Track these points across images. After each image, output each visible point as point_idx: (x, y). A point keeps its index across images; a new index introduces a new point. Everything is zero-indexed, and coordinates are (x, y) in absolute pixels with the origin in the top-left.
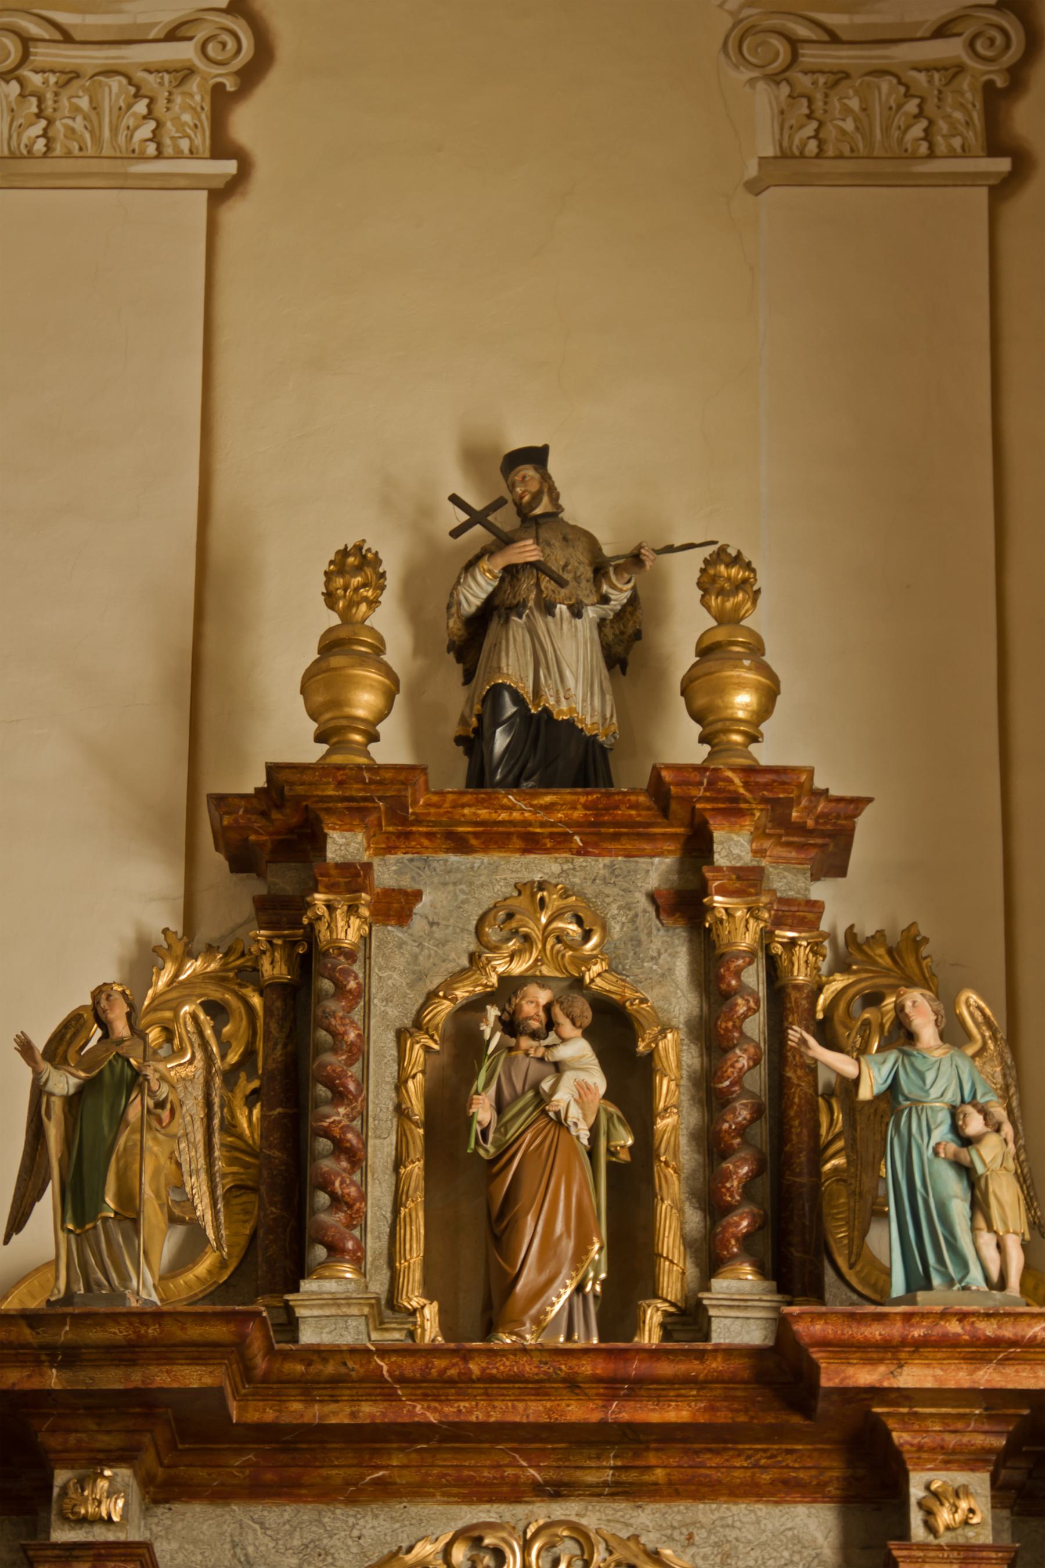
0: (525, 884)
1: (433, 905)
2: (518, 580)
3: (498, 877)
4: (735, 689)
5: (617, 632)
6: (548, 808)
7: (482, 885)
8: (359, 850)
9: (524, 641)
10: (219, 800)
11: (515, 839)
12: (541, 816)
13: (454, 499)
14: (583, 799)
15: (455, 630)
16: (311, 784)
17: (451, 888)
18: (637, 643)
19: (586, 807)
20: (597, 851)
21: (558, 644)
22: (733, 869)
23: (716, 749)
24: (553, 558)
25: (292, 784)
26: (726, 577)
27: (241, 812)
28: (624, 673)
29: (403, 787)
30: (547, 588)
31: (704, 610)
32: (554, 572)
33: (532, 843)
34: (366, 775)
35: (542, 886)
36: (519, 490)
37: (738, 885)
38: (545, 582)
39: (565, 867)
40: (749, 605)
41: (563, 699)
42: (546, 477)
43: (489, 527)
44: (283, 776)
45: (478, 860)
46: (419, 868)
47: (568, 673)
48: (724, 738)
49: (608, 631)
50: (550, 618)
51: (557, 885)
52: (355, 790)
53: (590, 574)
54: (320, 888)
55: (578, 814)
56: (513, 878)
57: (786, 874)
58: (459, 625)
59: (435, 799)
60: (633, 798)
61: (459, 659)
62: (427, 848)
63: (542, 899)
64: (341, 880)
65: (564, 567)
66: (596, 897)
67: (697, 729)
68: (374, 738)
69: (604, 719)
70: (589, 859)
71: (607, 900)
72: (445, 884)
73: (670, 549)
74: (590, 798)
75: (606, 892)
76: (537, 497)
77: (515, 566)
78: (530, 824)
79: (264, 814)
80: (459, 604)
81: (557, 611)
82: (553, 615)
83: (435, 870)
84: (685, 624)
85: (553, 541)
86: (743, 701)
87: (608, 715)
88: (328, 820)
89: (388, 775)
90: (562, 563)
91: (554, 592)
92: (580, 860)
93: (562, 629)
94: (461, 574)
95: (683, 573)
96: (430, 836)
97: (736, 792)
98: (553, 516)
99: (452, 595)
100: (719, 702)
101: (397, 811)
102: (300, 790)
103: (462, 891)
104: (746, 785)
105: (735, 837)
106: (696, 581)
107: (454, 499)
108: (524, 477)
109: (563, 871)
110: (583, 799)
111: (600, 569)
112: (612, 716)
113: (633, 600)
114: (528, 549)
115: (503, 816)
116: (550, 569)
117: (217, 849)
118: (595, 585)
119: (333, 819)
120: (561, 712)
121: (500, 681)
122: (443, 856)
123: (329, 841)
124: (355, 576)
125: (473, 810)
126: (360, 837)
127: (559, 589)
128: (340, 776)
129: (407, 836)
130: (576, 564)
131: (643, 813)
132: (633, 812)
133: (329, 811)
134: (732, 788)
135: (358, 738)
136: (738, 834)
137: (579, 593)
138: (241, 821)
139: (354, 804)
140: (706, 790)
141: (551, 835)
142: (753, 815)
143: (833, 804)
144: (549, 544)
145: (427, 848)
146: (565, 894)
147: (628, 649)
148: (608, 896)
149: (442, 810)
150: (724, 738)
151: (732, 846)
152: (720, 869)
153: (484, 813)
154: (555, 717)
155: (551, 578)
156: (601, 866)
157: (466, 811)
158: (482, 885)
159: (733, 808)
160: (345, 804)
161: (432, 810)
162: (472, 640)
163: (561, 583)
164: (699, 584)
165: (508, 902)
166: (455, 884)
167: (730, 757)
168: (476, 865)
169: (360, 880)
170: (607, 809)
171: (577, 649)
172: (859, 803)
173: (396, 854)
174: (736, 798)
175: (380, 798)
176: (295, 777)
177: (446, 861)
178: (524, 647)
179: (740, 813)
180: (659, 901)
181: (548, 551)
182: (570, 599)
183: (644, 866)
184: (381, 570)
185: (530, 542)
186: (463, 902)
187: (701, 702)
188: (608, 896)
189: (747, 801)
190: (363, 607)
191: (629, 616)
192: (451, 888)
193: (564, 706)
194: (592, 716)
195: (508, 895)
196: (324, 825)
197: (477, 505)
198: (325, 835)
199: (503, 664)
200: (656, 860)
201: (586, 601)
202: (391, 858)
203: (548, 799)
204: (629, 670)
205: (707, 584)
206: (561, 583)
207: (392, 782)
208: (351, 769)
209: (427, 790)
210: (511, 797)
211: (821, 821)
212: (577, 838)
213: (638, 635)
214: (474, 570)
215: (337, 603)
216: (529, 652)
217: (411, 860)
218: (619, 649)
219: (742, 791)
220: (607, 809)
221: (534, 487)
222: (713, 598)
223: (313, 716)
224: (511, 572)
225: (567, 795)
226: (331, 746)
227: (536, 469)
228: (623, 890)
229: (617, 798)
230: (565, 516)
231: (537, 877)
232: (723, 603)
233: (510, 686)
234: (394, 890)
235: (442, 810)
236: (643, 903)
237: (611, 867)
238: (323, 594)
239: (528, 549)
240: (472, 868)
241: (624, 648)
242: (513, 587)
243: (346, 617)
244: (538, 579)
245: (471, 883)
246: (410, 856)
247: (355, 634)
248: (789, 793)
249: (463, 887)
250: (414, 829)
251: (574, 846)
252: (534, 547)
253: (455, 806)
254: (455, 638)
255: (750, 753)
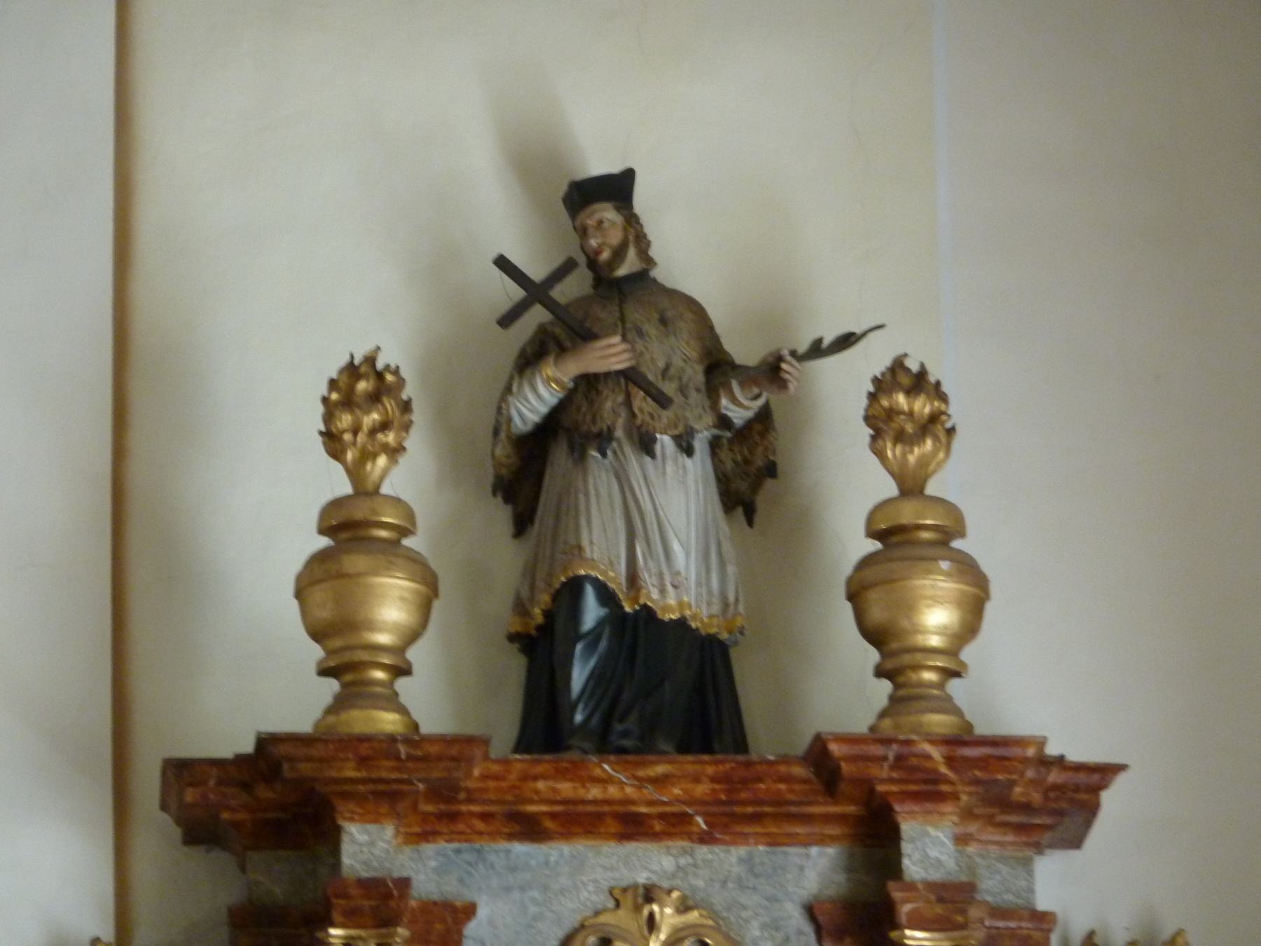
0: (625, 890)
1: (491, 923)
2: (598, 392)
3: (584, 879)
4: (929, 606)
5: (739, 458)
6: (660, 782)
7: (562, 891)
8: (388, 851)
9: (610, 496)
10: (180, 771)
11: (609, 820)
12: (649, 792)
13: (503, 263)
14: (710, 770)
15: (503, 459)
16: (320, 760)
17: (516, 895)
18: (769, 483)
19: (713, 780)
20: (727, 838)
21: (661, 500)
22: (932, 886)
23: (902, 692)
24: (647, 356)
25: (292, 760)
26: (907, 408)
27: (212, 783)
28: (750, 523)
29: (453, 764)
30: (641, 410)
31: (874, 460)
32: (651, 384)
33: (633, 826)
34: (403, 749)
35: (650, 894)
36: (593, 243)
37: (939, 909)
38: (641, 401)
39: (682, 861)
40: (941, 455)
41: (670, 588)
42: (632, 220)
43: (550, 305)
44: (281, 750)
45: (557, 852)
46: (469, 864)
47: (676, 547)
48: (913, 676)
49: (725, 455)
50: (647, 459)
51: (669, 892)
52: (385, 770)
53: (700, 378)
54: (337, 917)
55: (702, 789)
56: (606, 879)
57: (1000, 866)
58: (509, 449)
59: (495, 768)
60: (783, 769)
61: (508, 499)
62: (481, 833)
63: (651, 916)
64: (366, 903)
65: (665, 373)
66: (729, 909)
67: (873, 656)
68: (402, 670)
69: (726, 605)
70: (716, 849)
71: (744, 914)
72: (508, 889)
73: (817, 350)
74: (721, 768)
75: (742, 900)
76: (619, 254)
77: (596, 376)
78: (633, 802)
79: (246, 787)
80: (510, 419)
81: (658, 448)
82: (651, 454)
83: (492, 866)
84: (846, 483)
85: (646, 327)
86: (936, 619)
87: (731, 598)
88: (343, 807)
89: (434, 749)
90: (661, 364)
91: (652, 416)
92: (703, 851)
93: (664, 473)
94: (511, 379)
95: (841, 388)
96: (484, 817)
97: (935, 771)
98: (642, 278)
99: (499, 409)
100: (904, 623)
101: (445, 792)
102: (306, 769)
103: (534, 901)
104: (950, 761)
105: (932, 831)
106: (862, 413)
107: (503, 263)
108: (601, 222)
109: (679, 867)
110: (710, 770)
111: (718, 367)
112: (737, 600)
113: (764, 416)
114: (613, 351)
115: (595, 792)
116: (645, 378)
117: (164, 807)
118: (709, 397)
119: (352, 806)
120: (667, 608)
121: (582, 572)
122: (503, 845)
123: (345, 838)
124: (368, 412)
125: (551, 783)
126: (389, 831)
127: (660, 411)
128: (364, 750)
129: (453, 817)
130: (681, 363)
131: (797, 787)
132: (782, 787)
133: (345, 796)
134: (928, 764)
135: (379, 675)
136: (936, 827)
137: (688, 414)
138: (212, 796)
139: (381, 787)
140: (892, 768)
141: (662, 816)
142: (958, 799)
143: (1070, 774)
144: (640, 333)
145: (481, 833)
146: (684, 907)
147: (756, 486)
148: (745, 908)
149: (504, 784)
150: (913, 676)
151: (930, 847)
152: (911, 887)
153: (566, 788)
154: (660, 615)
155: (648, 393)
156: (734, 860)
157: (541, 785)
158: (562, 891)
159: (929, 792)
160: (371, 787)
161: (491, 784)
162: (527, 475)
163: (662, 401)
164: (869, 419)
165: (603, 919)
166: (522, 889)
167: (923, 711)
168: (552, 859)
169: (393, 904)
170: (744, 781)
171: (687, 503)
172: (1105, 773)
173: (435, 841)
174: (937, 779)
175: (420, 780)
176: (301, 751)
177: (508, 852)
178: (612, 506)
179: (940, 797)
180: (821, 918)
181: (640, 346)
182: (676, 426)
183: (797, 860)
184: (404, 397)
185: (616, 339)
186: (535, 918)
187: (877, 614)
188: (745, 908)
189: (952, 783)
190: (382, 461)
191: (757, 438)
192: (516, 895)
193: (672, 601)
194: (709, 604)
195: (600, 907)
196: (337, 816)
197: (537, 272)
198: (338, 830)
199: (585, 543)
200: (814, 850)
201: (697, 426)
202: (429, 848)
203: (660, 769)
204: (758, 519)
205: (881, 422)
206: (662, 401)
207: (439, 758)
208: (381, 741)
209: (486, 758)
210: (606, 767)
211: (1052, 795)
212: (699, 820)
213: (771, 470)
214: (533, 374)
215: (343, 451)
216: (619, 512)
217: (458, 851)
218: (742, 486)
219: (943, 769)
220: (744, 781)
221: (615, 237)
222: (889, 445)
223: (318, 634)
224: (589, 383)
225: (689, 763)
226: (345, 686)
227: (618, 209)
228: (768, 899)
229: (759, 768)
230: (656, 273)
231: (642, 878)
232: (904, 455)
233: (597, 579)
234: (435, 903)
235: (504, 784)
236: (796, 920)
237: (748, 861)
238: (321, 433)
239: (613, 351)
240: (547, 863)
241: (751, 476)
242: (591, 403)
243: (355, 473)
244: (628, 395)
245: (545, 888)
246: (455, 845)
247: (378, 514)
248: (1010, 773)
249: (535, 893)
250: (464, 808)
251: (695, 829)
252: (624, 346)
253: (525, 777)
254: (504, 471)
255: (949, 698)
